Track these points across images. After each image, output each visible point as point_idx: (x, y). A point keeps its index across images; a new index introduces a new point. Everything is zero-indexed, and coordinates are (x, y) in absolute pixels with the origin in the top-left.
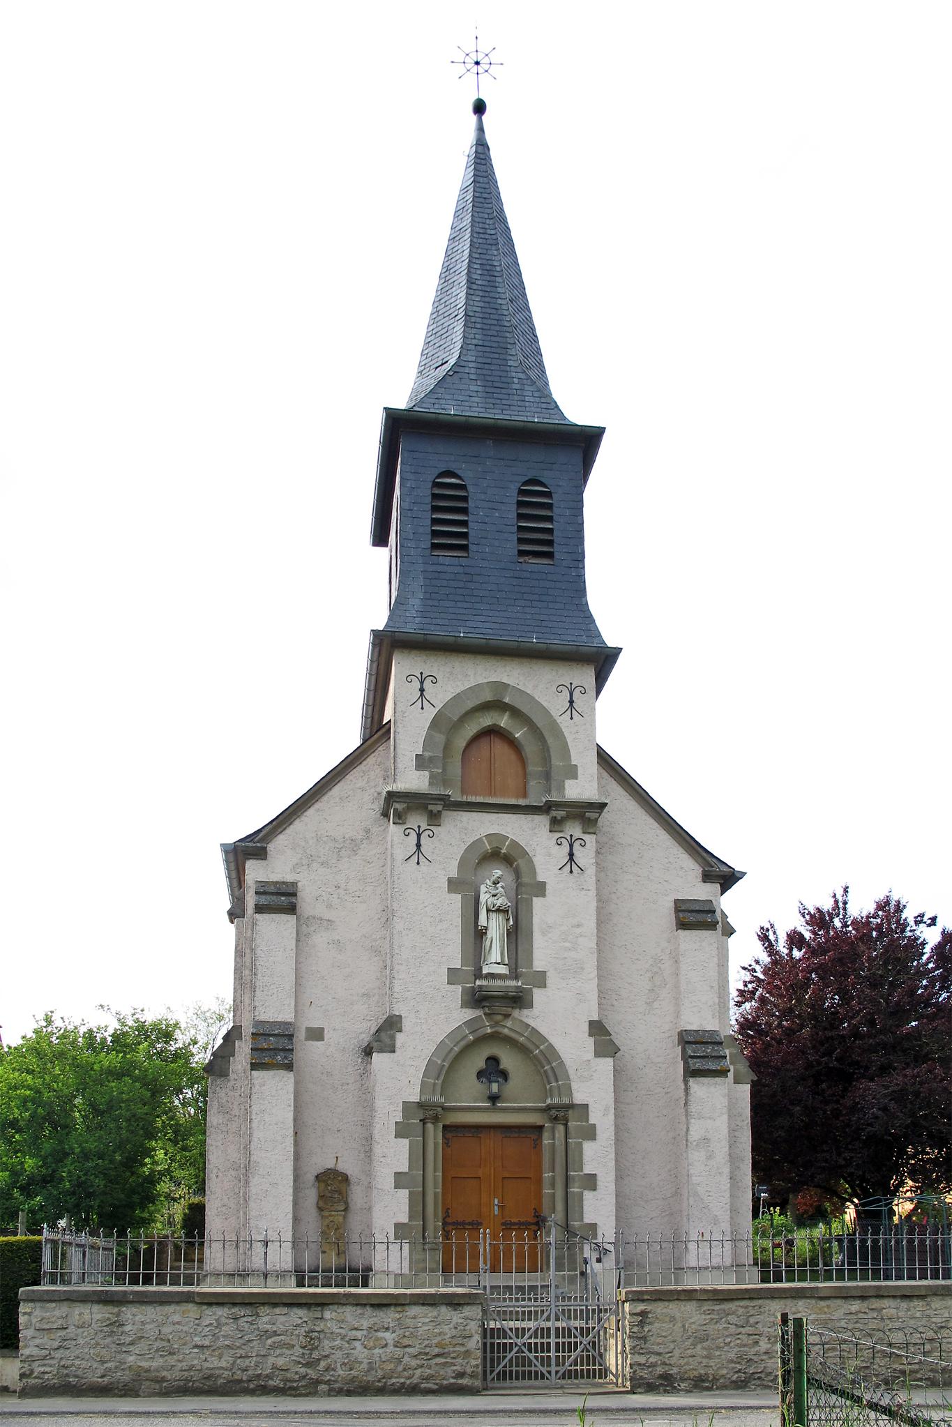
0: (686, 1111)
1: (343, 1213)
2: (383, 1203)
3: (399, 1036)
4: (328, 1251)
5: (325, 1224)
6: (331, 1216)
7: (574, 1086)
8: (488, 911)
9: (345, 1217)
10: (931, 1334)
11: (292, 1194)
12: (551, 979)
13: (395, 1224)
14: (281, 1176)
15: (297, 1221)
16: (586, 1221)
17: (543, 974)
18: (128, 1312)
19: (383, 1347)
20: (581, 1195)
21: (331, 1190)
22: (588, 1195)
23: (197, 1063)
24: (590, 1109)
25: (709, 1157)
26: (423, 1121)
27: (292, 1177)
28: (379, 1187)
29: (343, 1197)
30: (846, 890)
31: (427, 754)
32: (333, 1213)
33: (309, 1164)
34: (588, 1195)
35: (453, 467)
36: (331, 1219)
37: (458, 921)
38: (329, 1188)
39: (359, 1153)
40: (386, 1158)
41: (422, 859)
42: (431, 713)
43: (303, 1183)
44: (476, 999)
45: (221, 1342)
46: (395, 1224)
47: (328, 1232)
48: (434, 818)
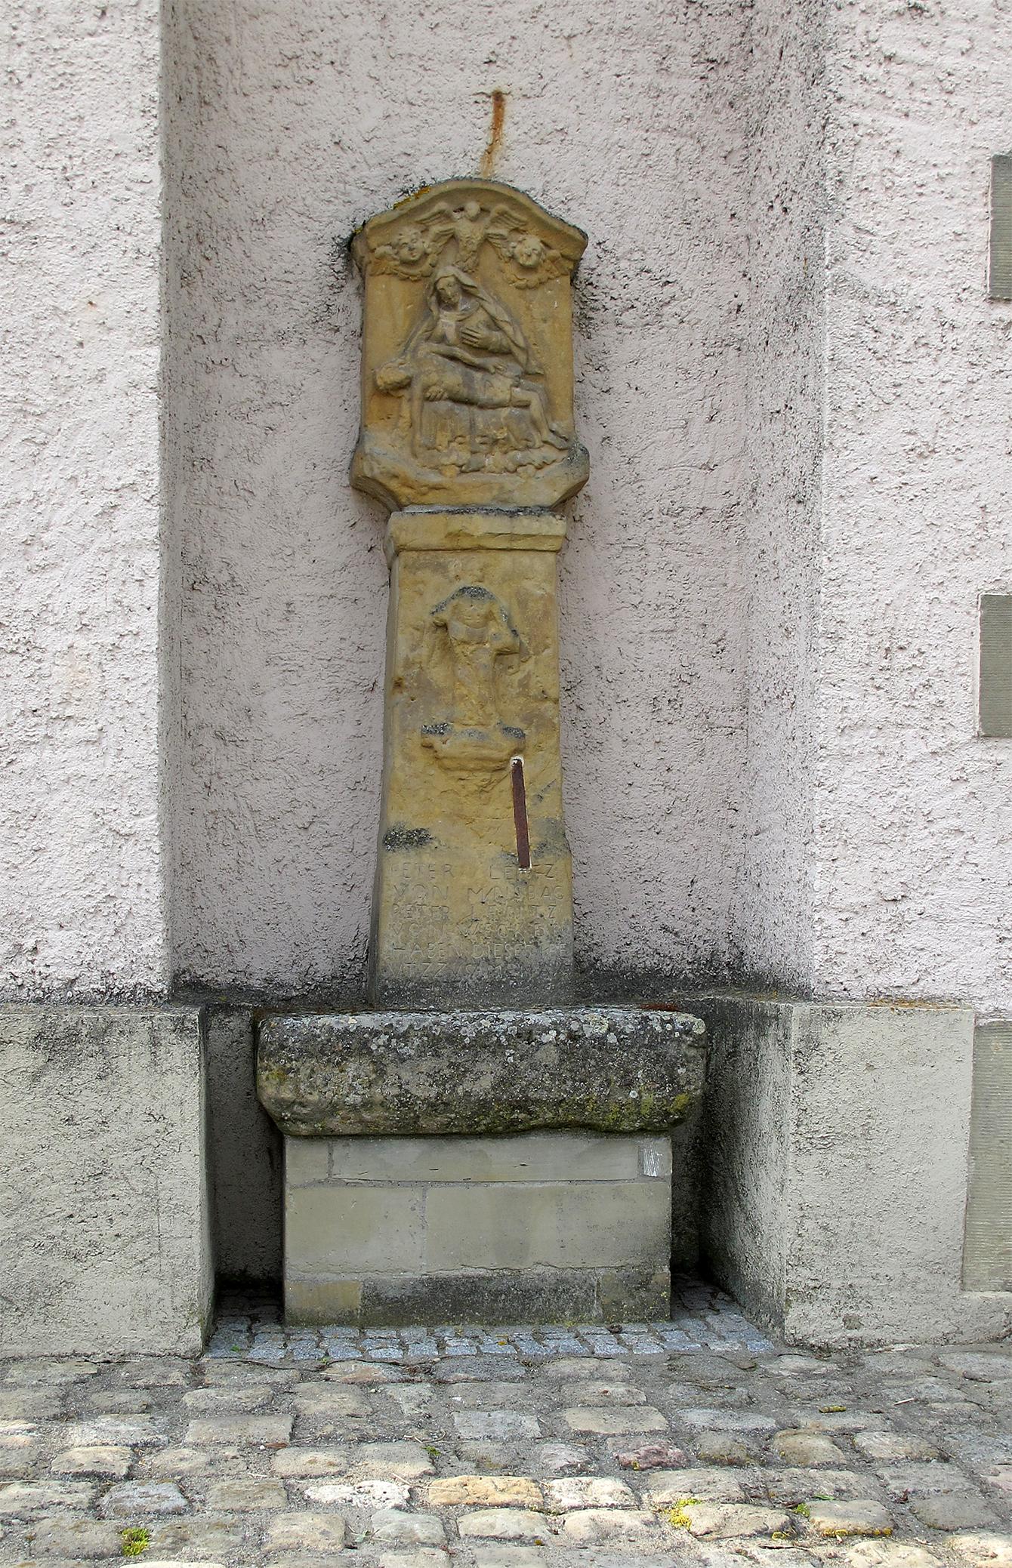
0: (310, 1184)
1: (556, 526)
2: (893, 421)
4: (437, 828)
5: (417, 610)
6: (460, 546)
9: (561, 576)
11: (151, 320)
13: (988, 602)
14: (59, 161)
15: (204, 600)
21: (466, 340)
23: (277, 1341)
27: (151, 170)
28: (870, 278)
29: (549, 406)
32: (479, 525)
33: (288, 148)
36: (464, 569)
38: (448, 322)
39: (663, 69)
40: (925, 30)
43: (248, 296)
46: (988, 602)
47: (438, 674)
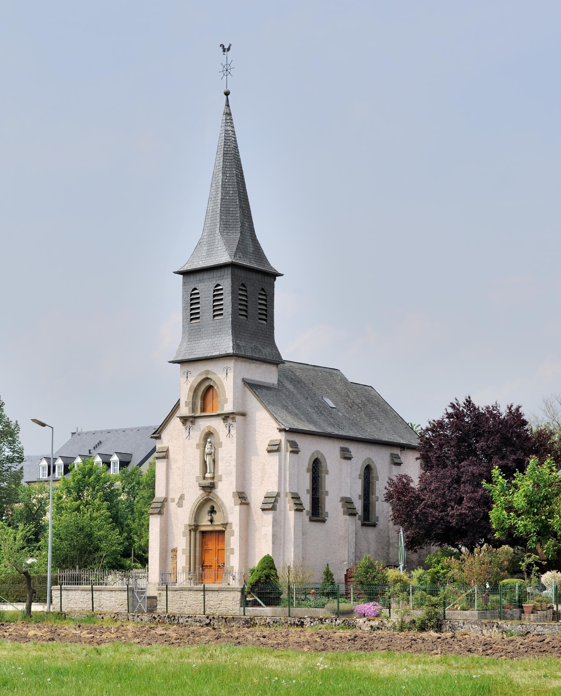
3: (184, 501)
7: (229, 516)
8: (206, 455)
10: (219, 602)
12: (224, 478)
16: (231, 565)
17: (221, 476)
18: (70, 592)
19: (512, 641)
20: (229, 556)
22: (231, 556)
24: (233, 524)
25: (267, 541)
26: (190, 530)
30: (469, 397)
31: (188, 401)
34: (231, 556)
35: (218, 282)
37: (199, 459)
41: (190, 438)
42: (189, 384)
44: (204, 488)
45: (85, 600)
48: (193, 422)
